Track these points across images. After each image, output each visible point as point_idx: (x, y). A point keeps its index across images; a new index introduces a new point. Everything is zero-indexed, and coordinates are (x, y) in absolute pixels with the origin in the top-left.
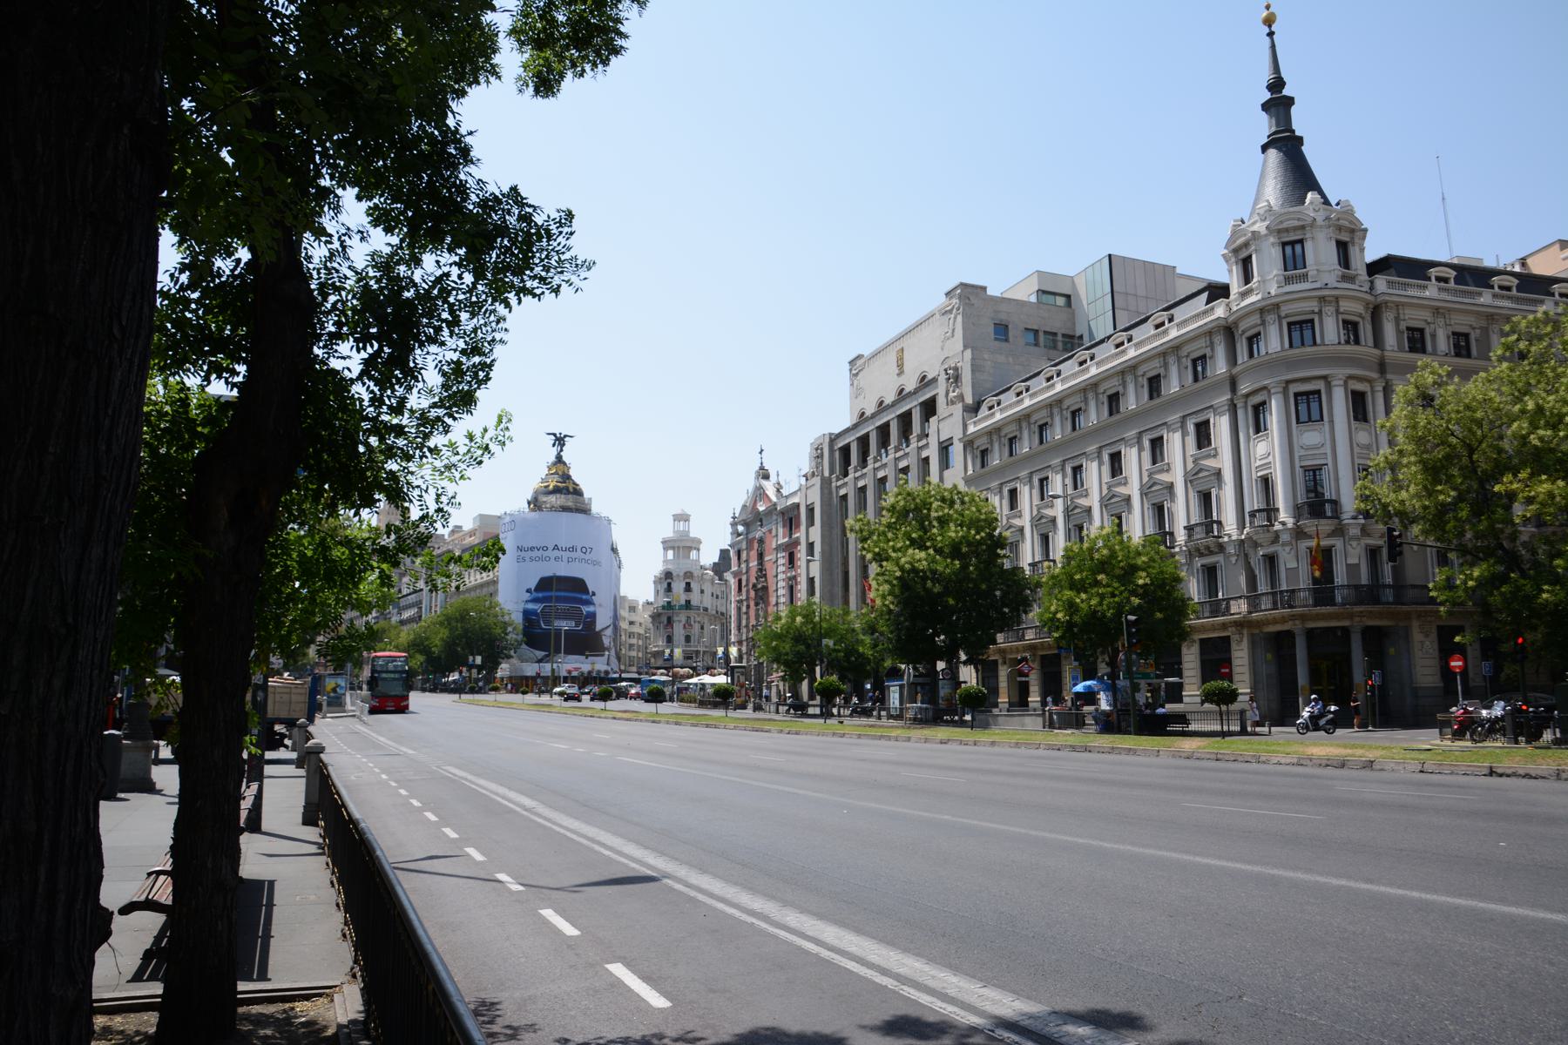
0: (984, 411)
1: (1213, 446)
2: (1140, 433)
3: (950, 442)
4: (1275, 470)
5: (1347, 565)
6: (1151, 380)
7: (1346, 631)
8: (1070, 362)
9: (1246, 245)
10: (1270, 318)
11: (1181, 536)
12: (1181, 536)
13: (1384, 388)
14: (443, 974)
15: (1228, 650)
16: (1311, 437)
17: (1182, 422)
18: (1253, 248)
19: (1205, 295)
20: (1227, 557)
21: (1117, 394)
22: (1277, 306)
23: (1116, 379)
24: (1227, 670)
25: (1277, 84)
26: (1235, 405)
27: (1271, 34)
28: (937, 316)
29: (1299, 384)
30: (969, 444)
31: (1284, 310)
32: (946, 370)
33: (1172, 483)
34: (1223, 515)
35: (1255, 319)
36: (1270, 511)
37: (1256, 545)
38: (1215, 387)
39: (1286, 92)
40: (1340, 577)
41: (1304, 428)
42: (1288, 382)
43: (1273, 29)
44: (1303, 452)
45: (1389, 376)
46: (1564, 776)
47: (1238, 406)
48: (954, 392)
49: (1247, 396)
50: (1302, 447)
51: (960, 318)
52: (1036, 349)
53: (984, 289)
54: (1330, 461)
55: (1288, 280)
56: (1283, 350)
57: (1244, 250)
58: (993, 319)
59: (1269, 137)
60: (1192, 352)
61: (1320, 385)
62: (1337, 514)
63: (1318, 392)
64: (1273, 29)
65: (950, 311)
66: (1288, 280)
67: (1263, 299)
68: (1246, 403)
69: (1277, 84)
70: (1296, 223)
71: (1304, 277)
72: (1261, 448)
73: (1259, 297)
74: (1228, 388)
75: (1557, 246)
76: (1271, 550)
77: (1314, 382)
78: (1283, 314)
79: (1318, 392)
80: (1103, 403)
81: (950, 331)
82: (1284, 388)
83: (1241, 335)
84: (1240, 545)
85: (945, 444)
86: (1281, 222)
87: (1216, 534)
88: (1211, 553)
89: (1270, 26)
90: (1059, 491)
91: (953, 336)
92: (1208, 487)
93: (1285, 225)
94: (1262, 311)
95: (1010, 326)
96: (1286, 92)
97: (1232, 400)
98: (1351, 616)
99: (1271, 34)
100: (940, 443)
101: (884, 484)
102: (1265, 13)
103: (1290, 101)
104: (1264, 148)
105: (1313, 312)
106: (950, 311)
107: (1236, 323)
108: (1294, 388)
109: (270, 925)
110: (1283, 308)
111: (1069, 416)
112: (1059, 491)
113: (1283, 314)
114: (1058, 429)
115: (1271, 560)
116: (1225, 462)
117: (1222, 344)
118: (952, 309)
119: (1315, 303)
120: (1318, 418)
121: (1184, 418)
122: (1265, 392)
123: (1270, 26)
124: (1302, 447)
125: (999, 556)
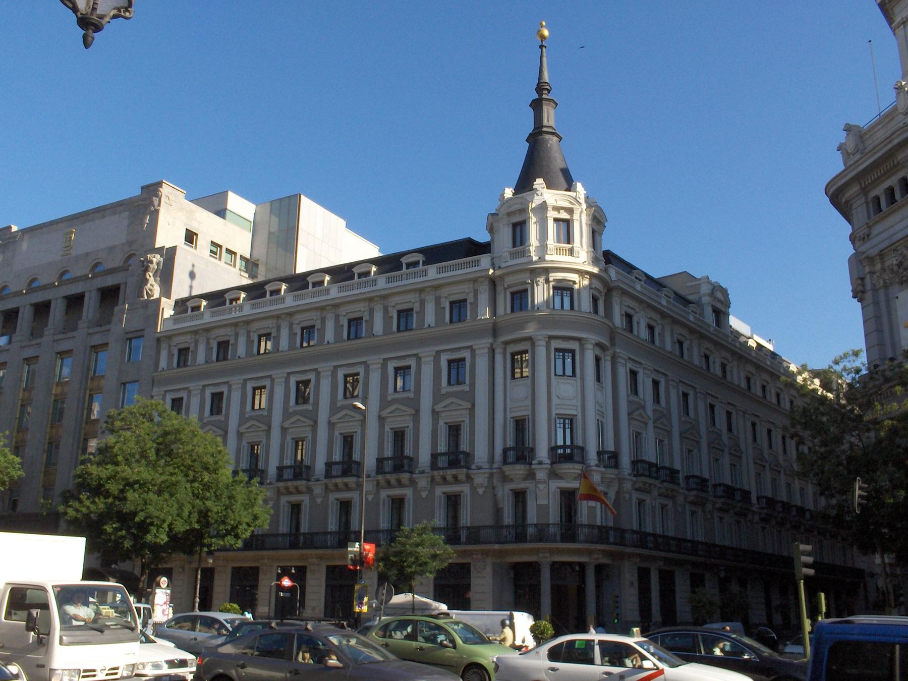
5: (588, 506)
7: (582, 566)
14: (52, 616)
26: (494, 351)
29: (560, 341)
38: (477, 333)
41: (560, 381)
42: (551, 338)
46: (905, 264)
49: (507, 343)
52: (232, 268)
54: (579, 417)
56: (506, 314)
58: (185, 224)
61: (574, 345)
62: (583, 461)
68: (505, 349)
76: (522, 486)
77: (571, 342)
79: (573, 352)
82: (547, 343)
83: (505, 289)
97: (492, 344)
98: (590, 552)
101: (186, 356)
108: (555, 344)
109: (316, 441)
120: (562, 374)
125: (99, 497)
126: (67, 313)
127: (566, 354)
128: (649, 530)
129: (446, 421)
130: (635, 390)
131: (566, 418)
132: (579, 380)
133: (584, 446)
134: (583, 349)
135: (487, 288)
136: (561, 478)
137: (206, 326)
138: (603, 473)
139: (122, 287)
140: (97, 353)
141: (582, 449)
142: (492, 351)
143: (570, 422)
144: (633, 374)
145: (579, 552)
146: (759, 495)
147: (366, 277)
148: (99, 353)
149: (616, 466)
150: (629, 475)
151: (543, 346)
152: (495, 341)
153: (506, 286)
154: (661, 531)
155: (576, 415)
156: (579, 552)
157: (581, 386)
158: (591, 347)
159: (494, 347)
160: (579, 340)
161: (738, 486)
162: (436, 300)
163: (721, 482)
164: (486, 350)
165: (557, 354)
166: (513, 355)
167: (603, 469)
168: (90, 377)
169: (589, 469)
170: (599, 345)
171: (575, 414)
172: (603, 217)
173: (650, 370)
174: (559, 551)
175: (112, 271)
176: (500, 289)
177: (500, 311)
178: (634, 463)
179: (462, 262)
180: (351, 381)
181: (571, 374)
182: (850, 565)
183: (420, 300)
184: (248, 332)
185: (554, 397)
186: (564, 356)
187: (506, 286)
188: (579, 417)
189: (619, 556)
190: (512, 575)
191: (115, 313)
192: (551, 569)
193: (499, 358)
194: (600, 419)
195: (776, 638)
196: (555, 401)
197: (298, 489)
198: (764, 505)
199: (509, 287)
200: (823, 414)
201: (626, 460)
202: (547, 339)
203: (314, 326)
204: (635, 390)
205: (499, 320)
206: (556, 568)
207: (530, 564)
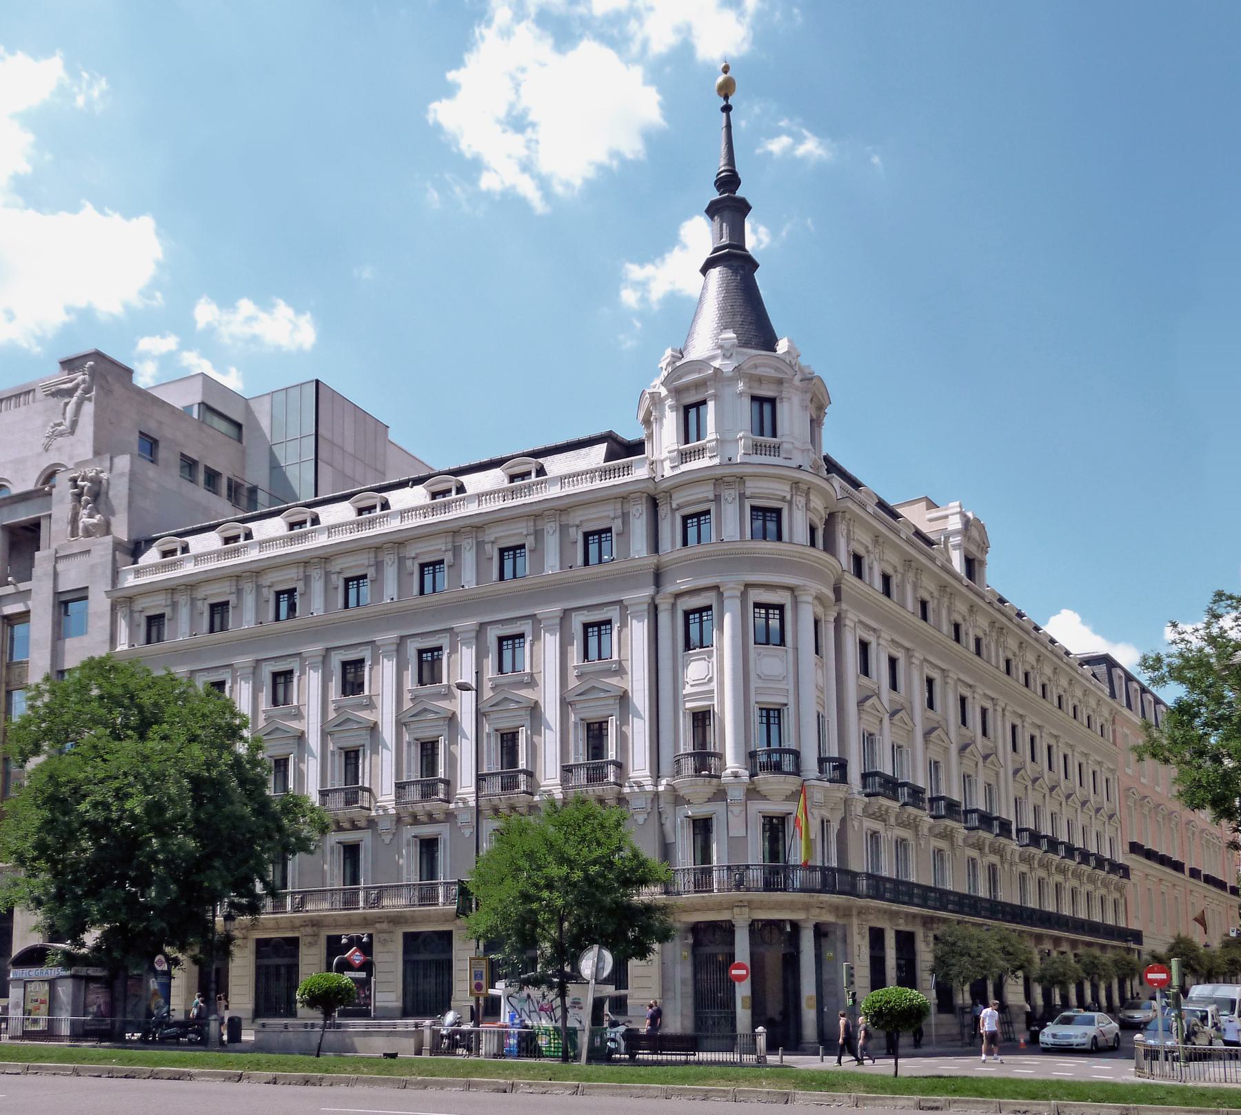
0: (151, 556)
1: (366, 692)
2: (403, 639)
3: (81, 595)
4: (722, 702)
6: (213, 607)
7: (795, 926)
8: (346, 504)
9: (700, 385)
10: (730, 494)
11: (466, 786)
12: (466, 786)
13: (835, 620)
15: (295, 954)
16: (771, 662)
17: (254, 668)
18: (711, 392)
19: (601, 449)
20: (377, 835)
21: (162, 616)
22: (741, 479)
23: (611, 507)
24: (1163, 976)
25: (729, 181)
26: (656, 607)
27: (727, 109)
28: (40, 394)
30: (123, 602)
31: (752, 487)
32: (74, 480)
33: (376, 724)
34: (540, 762)
35: (707, 491)
36: (704, 758)
37: (678, 800)
38: (628, 579)
39: (740, 193)
40: (797, 853)
42: (748, 586)
43: (730, 102)
44: (760, 684)
45: (844, 606)
47: (661, 608)
48: (91, 516)
49: (678, 596)
50: (759, 677)
51: (89, 408)
53: (129, 372)
54: (792, 707)
55: (757, 448)
57: (693, 392)
59: (716, 250)
60: (501, 537)
63: (781, 608)
64: (730, 102)
65: (70, 393)
66: (757, 448)
67: (721, 465)
68: (674, 605)
69: (729, 181)
70: (772, 373)
71: (775, 450)
72: (696, 670)
73: (716, 461)
74: (651, 579)
75: (923, 504)
78: (748, 493)
79: (781, 608)
80: (139, 625)
81: (67, 423)
83: (673, 511)
84: (652, 800)
85: (64, 598)
86: (756, 366)
87: (441, 796)
88: (355, 827)
89: (726, 98)
90: (469, 677)
91: (72, 432)
92: (435, 733)
93: (760, 371)
94: (718, 481)
95: (161, 445)
96: (740, 193)
97: (653, 599)
98: (807, 907)
99: (727, 109)
100: (57, 594)
102: (721, 79)
103: (742, 208)
104: (704, 270)
105: (783, 499)
106: (70, 393)
107: (669, 493)
110: (748, 484)
111: (341, 584)
112: (469, 677)
113: (748, 493)
114: (391, 589)
115: (702, 827)
116: (638, 686)
117: (644, 516)
118: (77, 386)
119: (788, 488)
121: (566, 613)
122: (713, 594)
123: (726, 98)
124: (759, 677)
126: (10, 555)
127: (771, 611)
128: (885, 873)
129: (583, 716)
130: (865, 670)
131: (772, 709)
132: (790, 651)
133: (798, 749)
134: (796, 603)
135: (644, 508)
136: (765, 798)
137: (190, 579)
138: (827, 790)
139: (44, 524)
140: (12, 627)
141: (796, 754)
142: (654, 610)
143: (772, 716)
144: (864, 646)
145: (792, 906)
146: (1019, 827)
147: (370, 513)
148: (16, 627)
149: (844, 780)
150: (859, 793)
151: (737, 597)
152: (657, 592)
153: (674, 506)
154: (895, 873)
155: (786, 705)
156: (792, 906)
157: (678, 683)
158: (810, 599)
159: (657, 602)
160: (791, 589)
161: (995, 814)
162: (561, 530)
163: (975, 807)
164: (646, 607)
165: (757, 610)
166: (687, 614)
167: (827, 784)
168: (4, 664)
169: (806, 783)
170: (819, 598)
171: (785, 702)
172: (826, 398)
173: (887, 640)
174: (761, 906)
175: (25, 497)
176: (663, 511)
177: (665, 545)
178: (865, 776)
179: (607, 469)
180: (429, 659)
181: (778, 641)
182: (1123, 925)
183: (623, 513)
184: (327, 574)
185: (753, 676)
186: (767, 614)
187: (674, 506)
188: (792, 707)
189: (846, 912)
190: (690, 941)
191: (36, 562)
192: (750, 931)
193: (664, 618)
194: (821, 710)
195: (841, 1041)
196: (754, 683)
197: (339, 823)
198: (1027, 841)
199: (679, 507)
200: (157, 863)
201: (854, 772)
202: (743, 588)
203: (443, 560)
204: (865, 670)
205: (665, 559)
206: (760, 930)
207: (713, 926)
